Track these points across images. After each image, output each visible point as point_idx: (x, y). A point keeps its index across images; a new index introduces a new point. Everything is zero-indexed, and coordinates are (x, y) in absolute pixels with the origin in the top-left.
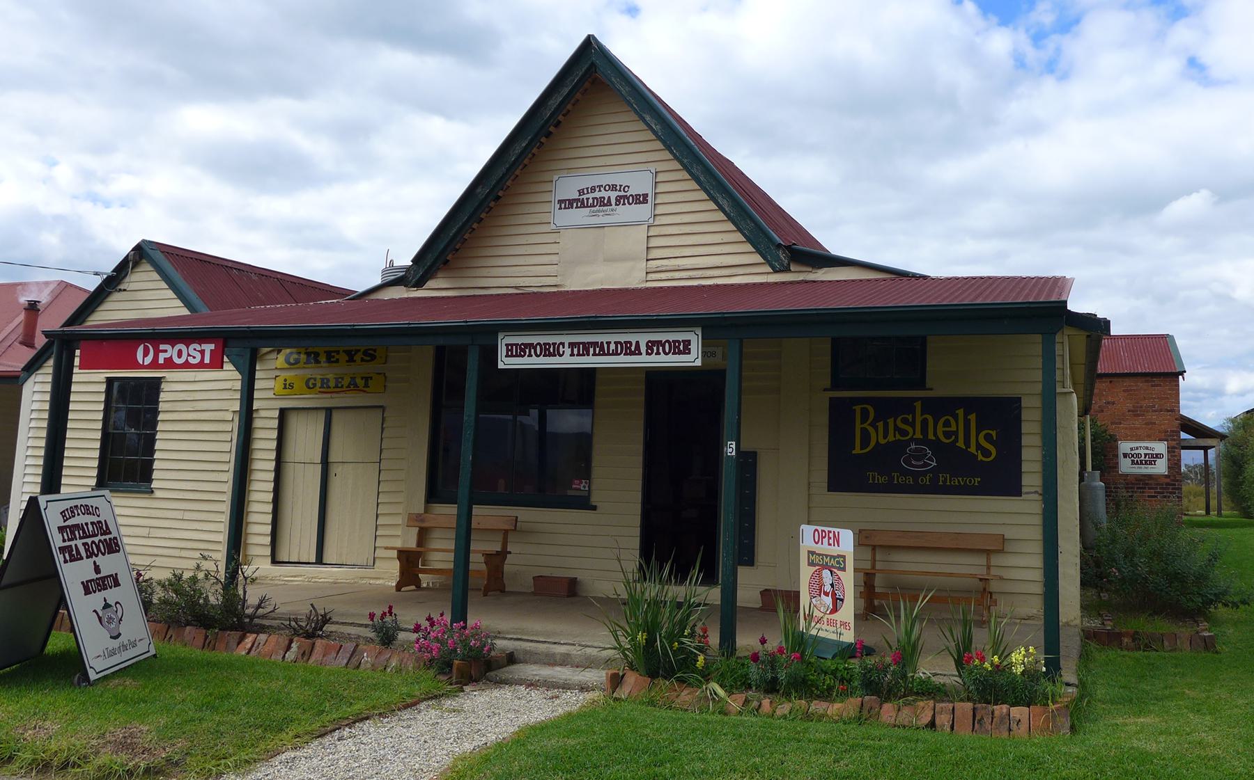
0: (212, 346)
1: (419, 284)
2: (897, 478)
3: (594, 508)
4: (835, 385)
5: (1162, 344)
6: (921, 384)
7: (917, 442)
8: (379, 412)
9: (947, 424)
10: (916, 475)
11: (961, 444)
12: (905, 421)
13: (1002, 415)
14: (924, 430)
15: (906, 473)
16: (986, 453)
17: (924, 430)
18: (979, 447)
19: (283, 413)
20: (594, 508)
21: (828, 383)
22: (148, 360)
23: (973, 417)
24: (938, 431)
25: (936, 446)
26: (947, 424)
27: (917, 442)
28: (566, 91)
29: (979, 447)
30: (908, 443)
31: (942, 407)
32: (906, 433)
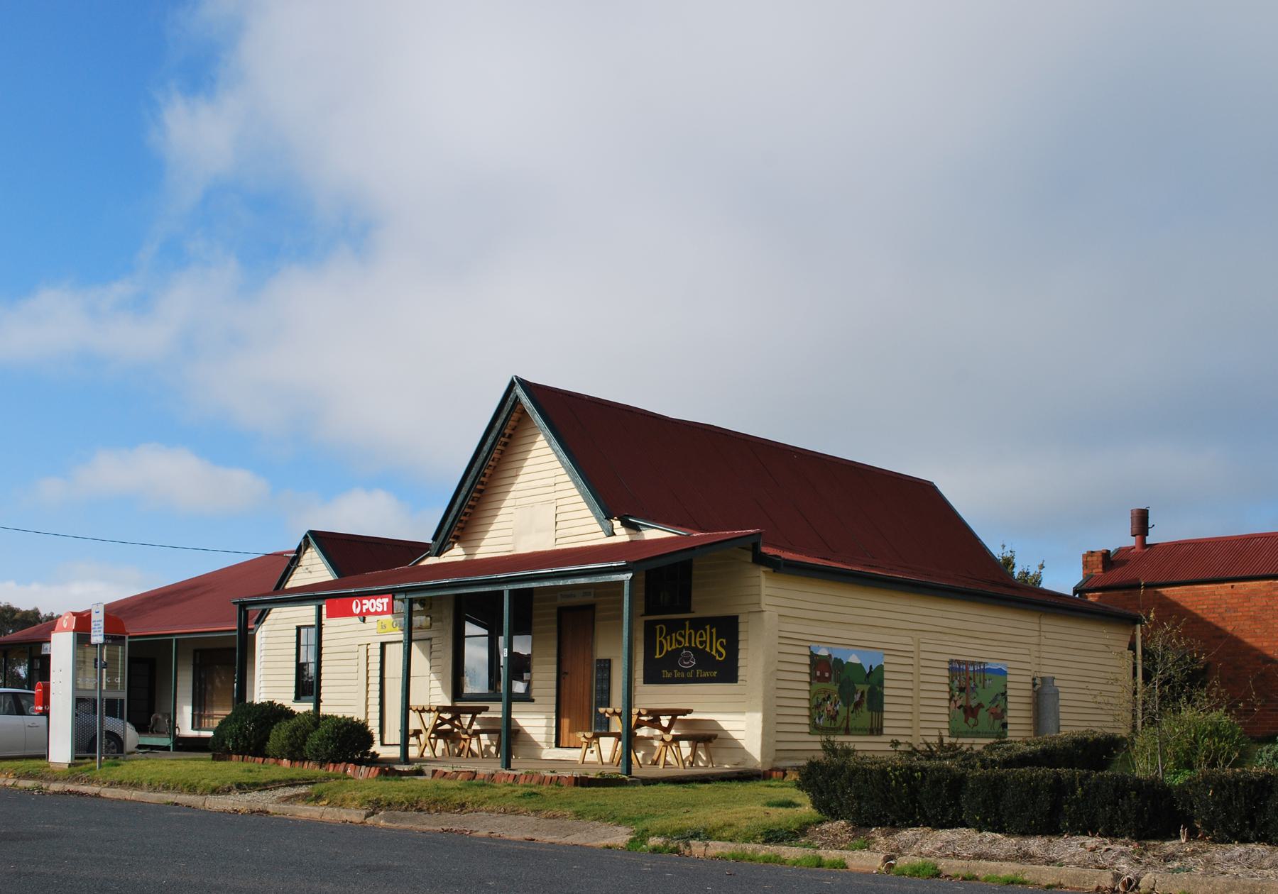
0: (630, 575)
1: (438, 554)
2: (678, 674)
3: (533, 701)
4: (648, 612)
5: (1088, 558)
6: (688, 610)
7: (687, 649)
8: (428, 643)
9: (701, 636)
10: (686, 671)
11: (708, 649)
12: (681, 635)
13: (729, 629)
14: (690, 642)
15: (681, 670)
16: (721, 655)
17: (690, 642)
18: (717, 651)
19: (383, 645)
20: (533, 701)
21: (642, 611)
22: (358, 611)
23: (714, 630)
24: (696, 642)
25: (695, 650)
26: (701, 636)
27: (687, 649)
28: (504, 416)
29: (717, 651)
30: (681, 650)
31: (698, 624)
32: (680, 643)
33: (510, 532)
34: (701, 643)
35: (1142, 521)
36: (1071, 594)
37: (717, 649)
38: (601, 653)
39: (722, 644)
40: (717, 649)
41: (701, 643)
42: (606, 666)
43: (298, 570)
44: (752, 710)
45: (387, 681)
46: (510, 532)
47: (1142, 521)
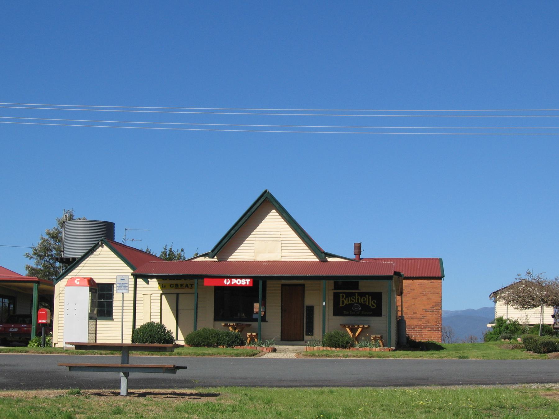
3: (267, 322)
6: (357, 289)
9: (364, 299)
11: (367, 304)
14: (358, 301)
16: (373, 306)
17: (358, 301)
21: (333, 288)
23: (370, 297)
25: (361, 304)
26: (364, 299)
27: (358, 303)
30: (354, 304)
31: (362, 295)
33: (253, 251)
34: (364, 301)
35: (358, 249)
36: (130, 342)
37: (372, 304)
38: (308, 302)
39: (374, 302)
40: (372, 304)
41: (364, 301)
42: (310, 310)
43: (92, 256)
44: (446, 312)
45: (163, 311)
46: (253, 251)
47: (358, 249)
